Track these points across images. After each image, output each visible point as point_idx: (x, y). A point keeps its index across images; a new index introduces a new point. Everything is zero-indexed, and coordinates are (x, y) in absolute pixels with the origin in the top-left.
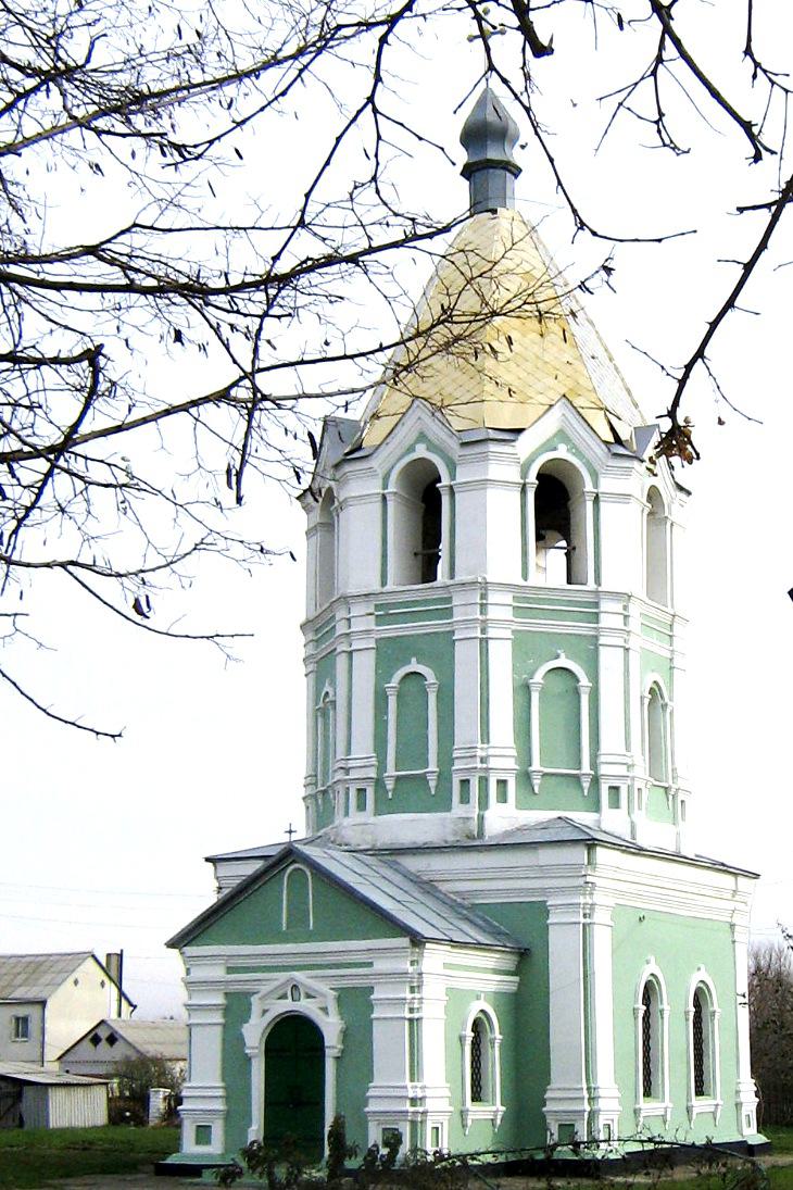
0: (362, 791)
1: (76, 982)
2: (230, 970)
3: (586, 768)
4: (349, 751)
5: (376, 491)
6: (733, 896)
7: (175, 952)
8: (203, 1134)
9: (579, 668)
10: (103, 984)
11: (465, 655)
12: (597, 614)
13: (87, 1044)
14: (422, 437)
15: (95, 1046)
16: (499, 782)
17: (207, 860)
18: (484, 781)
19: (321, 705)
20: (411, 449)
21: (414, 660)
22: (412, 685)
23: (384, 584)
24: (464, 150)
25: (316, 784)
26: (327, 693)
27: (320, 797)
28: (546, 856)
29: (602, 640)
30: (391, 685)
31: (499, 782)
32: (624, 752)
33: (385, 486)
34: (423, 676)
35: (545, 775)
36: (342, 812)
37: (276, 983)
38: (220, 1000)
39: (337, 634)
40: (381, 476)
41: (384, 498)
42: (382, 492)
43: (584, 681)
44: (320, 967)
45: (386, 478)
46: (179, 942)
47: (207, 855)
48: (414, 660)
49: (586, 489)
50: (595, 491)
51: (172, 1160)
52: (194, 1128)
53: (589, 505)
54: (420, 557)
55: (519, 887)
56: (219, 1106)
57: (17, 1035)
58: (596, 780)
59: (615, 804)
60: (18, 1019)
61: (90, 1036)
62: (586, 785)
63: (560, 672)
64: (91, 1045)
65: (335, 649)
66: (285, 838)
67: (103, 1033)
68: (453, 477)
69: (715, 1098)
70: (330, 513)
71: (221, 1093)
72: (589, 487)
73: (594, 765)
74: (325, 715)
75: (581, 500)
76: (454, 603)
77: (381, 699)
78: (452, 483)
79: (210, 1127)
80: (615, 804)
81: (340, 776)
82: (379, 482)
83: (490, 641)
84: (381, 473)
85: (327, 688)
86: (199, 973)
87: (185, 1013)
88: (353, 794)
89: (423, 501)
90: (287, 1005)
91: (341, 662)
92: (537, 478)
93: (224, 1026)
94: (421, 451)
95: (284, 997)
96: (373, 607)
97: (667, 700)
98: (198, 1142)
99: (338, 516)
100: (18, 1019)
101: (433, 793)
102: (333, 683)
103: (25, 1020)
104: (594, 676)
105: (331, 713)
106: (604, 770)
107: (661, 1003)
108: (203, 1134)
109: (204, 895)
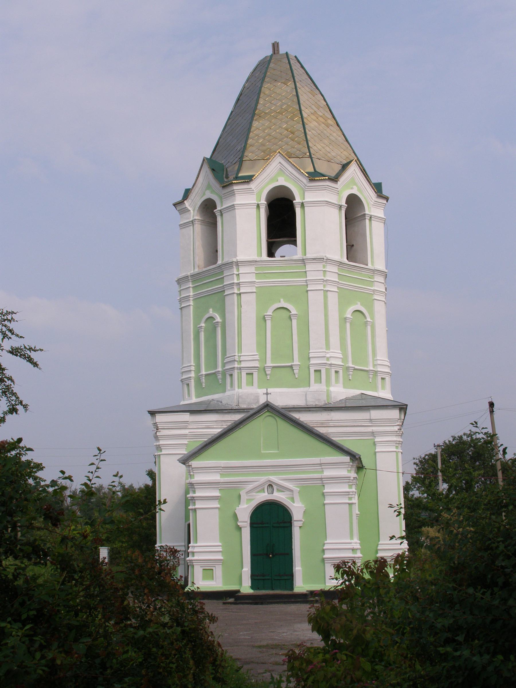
11: (315, 299)
12: (306, 272)
20: (204, 194)
22: (284, 313)
28: (375, 414)
35: (355, 369)
41: (258, 206)
42: (301, 201)
62: (220, 376)
63: (282, 310)
79: (212, 570)
82: (255, 196)
94: (282, 181)
98: (205, 578)
108: (208, 573)
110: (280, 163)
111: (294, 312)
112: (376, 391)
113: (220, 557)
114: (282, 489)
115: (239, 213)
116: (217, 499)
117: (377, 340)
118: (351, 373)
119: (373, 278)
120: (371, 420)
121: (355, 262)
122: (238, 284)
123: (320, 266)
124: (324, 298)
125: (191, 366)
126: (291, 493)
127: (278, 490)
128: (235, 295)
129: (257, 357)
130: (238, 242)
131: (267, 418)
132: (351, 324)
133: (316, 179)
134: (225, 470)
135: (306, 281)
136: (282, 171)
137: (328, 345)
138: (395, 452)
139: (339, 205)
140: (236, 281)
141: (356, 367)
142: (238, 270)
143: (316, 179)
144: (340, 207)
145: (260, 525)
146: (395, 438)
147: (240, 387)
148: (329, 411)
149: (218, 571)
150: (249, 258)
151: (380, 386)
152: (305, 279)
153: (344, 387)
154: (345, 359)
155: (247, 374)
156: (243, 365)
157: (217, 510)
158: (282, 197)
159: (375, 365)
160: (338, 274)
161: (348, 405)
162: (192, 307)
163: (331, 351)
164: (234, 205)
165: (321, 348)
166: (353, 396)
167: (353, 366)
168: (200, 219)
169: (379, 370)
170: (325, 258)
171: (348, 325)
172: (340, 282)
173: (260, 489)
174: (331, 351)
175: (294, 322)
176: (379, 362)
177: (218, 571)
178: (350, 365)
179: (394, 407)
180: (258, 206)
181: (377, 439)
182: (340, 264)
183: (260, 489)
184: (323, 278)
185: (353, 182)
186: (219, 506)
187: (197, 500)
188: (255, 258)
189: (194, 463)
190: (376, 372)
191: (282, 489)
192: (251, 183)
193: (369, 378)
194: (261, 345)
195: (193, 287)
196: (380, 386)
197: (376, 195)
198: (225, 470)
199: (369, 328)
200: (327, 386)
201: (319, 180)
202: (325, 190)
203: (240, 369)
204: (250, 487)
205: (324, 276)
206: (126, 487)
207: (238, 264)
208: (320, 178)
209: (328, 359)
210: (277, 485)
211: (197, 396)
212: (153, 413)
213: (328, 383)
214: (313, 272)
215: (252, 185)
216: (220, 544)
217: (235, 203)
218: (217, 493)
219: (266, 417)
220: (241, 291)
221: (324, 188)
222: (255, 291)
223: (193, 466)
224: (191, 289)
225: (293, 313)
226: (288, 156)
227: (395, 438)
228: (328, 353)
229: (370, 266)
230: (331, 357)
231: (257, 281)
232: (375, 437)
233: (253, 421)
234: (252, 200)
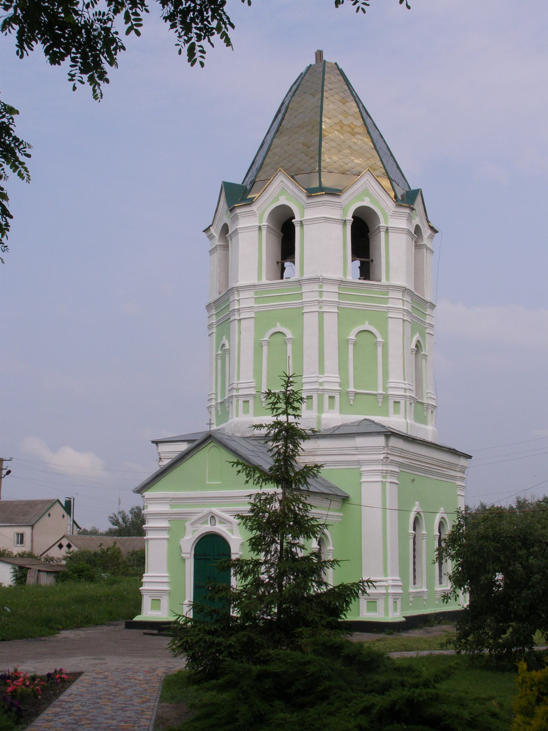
4: (238, 378)
9: (376, 330)
10: (63, 516)
11: (310, 322)
12: (302, 293)
13: (56, 547)
16: (330, 397)
17: (153, 442)
18: (321, 397)
20: (276, 199)
21: (367, 323)
22: (278, 337)
23: (260, 278)
28: (360, 441)
30: (265, 339)
31: (330, 397)
33: (261, 221)
35: (356, 393)
36: (234, 414)
37: (200, 515)
39: (231, 309)
41: (260, 228)
42: (258, 224)
45: (261, 215)
47: (153, 440)
48: (278, 324)
50: (386, 226)
51: (137, 618)
55: (357, 459)
60: (18, 534)
63: (275, 335)
64: (58, 548)
65: (230, 318)
66: (206, 429)
70: (226, 238)
72: (382, 224)
75: (377, 232)
78: (302, 219)
79: (160, 600)
82: (257, 218)
83: (325, 315)
90: (207, 528)
92: (352, 218)
94: (283, 201)
95: (206, 522)
98: (369, 609)
100: (18, 534)
102: (229, 338)
103: (22, 535)
104: (385, 335)
108: (156, 603)
110: (282, 181)
111: (289, 335)
112: (388, 416)
113: (166, 588)
114: (223, 521)
115: (241, 236)
116: (166, 530)
117: (391, 360)
118: (347, 399)
119: (388, 295)
120: (357, 448)
121: (369, 280)
122: (238, 310)
123: (315, 287)
124: (319, 320)
125: (212, 394)
126: (230, 525)
127: (221, 522)
128: (236, 321)
129: (253, 384)
130: (240, 267)
131: (214, 448)
132: (354, 345)
133: (313, 195)
134: (173, 501)
135: (302, 303)
136: (284, 191)
137: (322, 370)
138: (382, 482)
139: (343, 220)
140: (237, 307)
141: (358, 391)
143: (313, 195)
144: (345, 222)
145: (203, 557)
146: (380, 468)
147: (237, 416)
148: (316, 439)
149: (165, 602)
150: (252, 282)
151: (391, 410)
152: (301, 301)
153: (340, 413)
154: (343, 383)
156: (241, 392)
157: (166, 541)
159: (385, 388)
160: (339, 293)
161: (337, 432)
162: (214, 335)
163: (326, 375)
164: (237, 229)
165: (314, 373)
166: (352, 423)
167: (355, 390)
168: (223, 244)
169: (390, 393)
170: (321, 278)
171: (351, 347)
172: (340, 301)
173: (202, 520)
174: (326, 375)
175: (289, 347)
176: (391, 385)
177: (165, 602)
178: (351, 389)
179: (378, 433)
181: (363, 468)
183: (202, 520)
184: (319, 299)
185: (366, 192)
186: (167, 537)
187: (150, 530)
188: (255, 282)
189: (148, 494)
190: (386, 397)
191: (223, 521)
192: (253, 205)
193: (379, 402)
194: (257, 372)
195: (216, 314)
196: (391, 410)
197: (394, 204)
198: (173, 501)
199: (380, 350)
200: (318, 412)
201: (316, 195)
202: (324, 205)
203: (237, 396)
204: (195, 518)
205: (321, 297)
206: (487, 508)
207: (238, 289)
208: (317, 194)
209: (321, 384)
210: (218, 516)
211: (217, 426)
212: (156, 443)
213: (321, 409)
214: (309, 293)
215: (254, 208)
216: (167, 575)
217: (238, 227)
218: (165, 524)
219: (211, 448)
220: (241, 317)
221: (323, 204)
222: (253, 316)
223: (146, 497)
224: (214, 316)
225: (288, 337)
227: (380, 468)
228: (321, 377)
229: (384, 281)
230: (324, 382)
231: (256, 306)
232: (361, 465)
233: (199, 452)
234: (254, 222)
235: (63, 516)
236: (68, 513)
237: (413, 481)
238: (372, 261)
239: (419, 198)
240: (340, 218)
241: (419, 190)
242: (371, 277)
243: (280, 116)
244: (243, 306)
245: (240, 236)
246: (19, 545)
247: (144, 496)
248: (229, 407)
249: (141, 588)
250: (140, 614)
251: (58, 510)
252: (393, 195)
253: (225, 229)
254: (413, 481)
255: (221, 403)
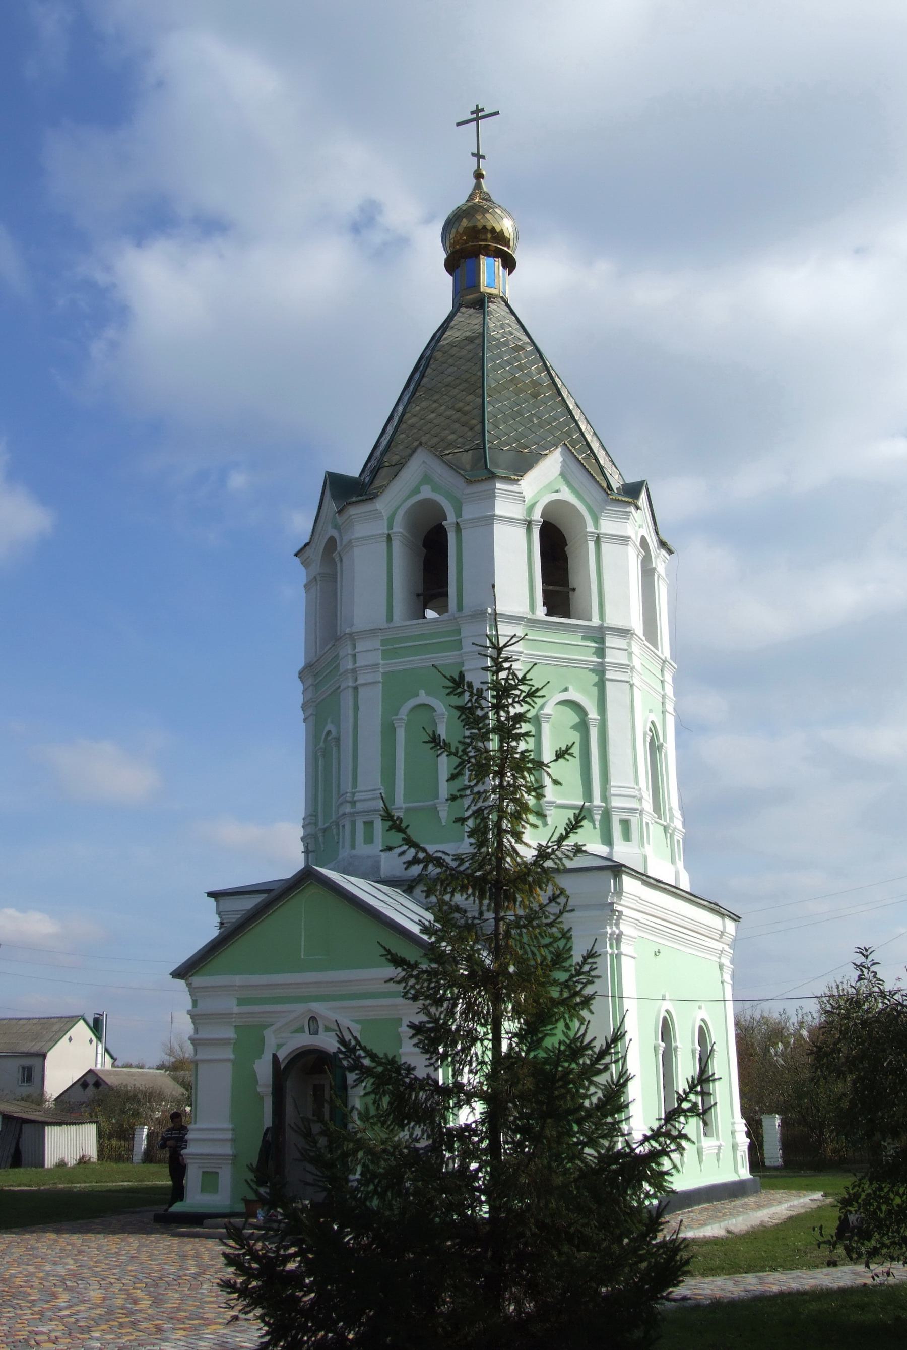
0: (369, 824)
1: (70, 1039)
2: (241, 1002)
3: (597, 801)
4: (355, 785)
5: (380, 532)
6: (721, 937)
7: (181, 983)
8: (210, 1180)
10: (91, 1041)
14: (427, 479)
15: (571, 728)
19: (322, 744)
20: (416, 491)
24: (303, 568)
25: (316, 824)
26: (329, 732)
27: (320, 835)
29: (608, 675)
32: (633, 785)
33: (390, 527)
34: (433, 708)
38: (230, 1033)
40: (385, 518)
41: (389, 538)
43: (593, 714)
44: (343, 997)
46: (183, 972)
48: (422, 692)
49: (589, 530)
52: (200, 1173)
53: (591, 545)
54: (422, 598)
56: (228, 1150)
57: (23, 1081)
58: (607, 815)
59: (627, 837)
60: (24, 1068)
61: (80, 1083)
64: (81, 1089)
67: (91, 1081)
68: (459, 514)
69: (718, 1139)
71: (229, 1135)
72: (590, 528)
73: (605, 798)
74: (326, 753)
76: (462, 635)
77: (389, 731)
79: (217, 1173)
80: (627, 837)
81: (348, 809)
84: (385, 514)
85: (329, 727)
86: (210, 1005)
87: (189, 1047)
88: (360, 826)
89: (424, 546)
91: (347, 699)
93: (234, 1062)
94: (426, 492)
95: (300, 1030)
96: (379, 643)
97: (661, 741)
98: (204, 1189)
99: (341, 560)
100: (24, 1068)
101: (444, 824)
105: (334, 749)
106: (615, 803)
107: (675, 1041)
108: (210, 1180)
109: (206, 927)
110: (424, 462)
121: (567, 615)
135: (461, 655)
139: (526, 520)
142: (354, 647)
147: (353, 847)
155: (365, 823)
156: (360, 806)
158: (564, 533)
164: (350, 541)
180: (389, 538)
182: (533, 623)
220: (359, 682)
223: (194, 985)
226: (440, 452)
235: (91, 1041)
236: (97, 1037)
237: (657, 953)
238: (574, 590)
239: (643, 495)
240: (521, 517)
241: (643, 482)
242: (572, 613)
243: (417, 376)
244: (362, 664)
245: (356, 551)
246: (25, 1084)
247: (191, 984)
248: (338, 834)
249: (183, 1152)
250: (182, 1200)
251: (81, 1031)
252: (605, 485)
253: (331, 544)
254: (657, 953)
255: (325, 830)
